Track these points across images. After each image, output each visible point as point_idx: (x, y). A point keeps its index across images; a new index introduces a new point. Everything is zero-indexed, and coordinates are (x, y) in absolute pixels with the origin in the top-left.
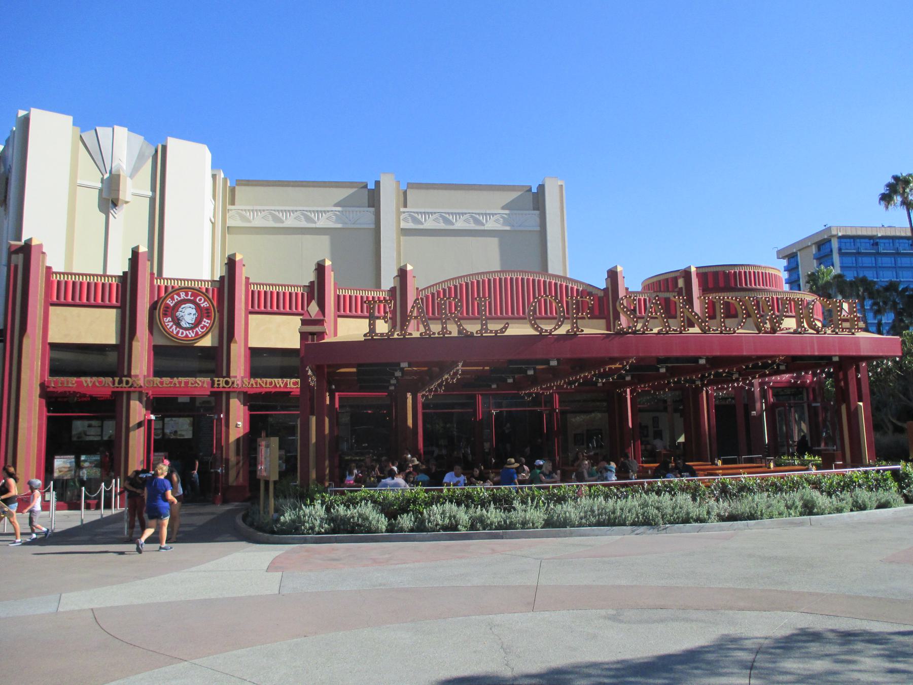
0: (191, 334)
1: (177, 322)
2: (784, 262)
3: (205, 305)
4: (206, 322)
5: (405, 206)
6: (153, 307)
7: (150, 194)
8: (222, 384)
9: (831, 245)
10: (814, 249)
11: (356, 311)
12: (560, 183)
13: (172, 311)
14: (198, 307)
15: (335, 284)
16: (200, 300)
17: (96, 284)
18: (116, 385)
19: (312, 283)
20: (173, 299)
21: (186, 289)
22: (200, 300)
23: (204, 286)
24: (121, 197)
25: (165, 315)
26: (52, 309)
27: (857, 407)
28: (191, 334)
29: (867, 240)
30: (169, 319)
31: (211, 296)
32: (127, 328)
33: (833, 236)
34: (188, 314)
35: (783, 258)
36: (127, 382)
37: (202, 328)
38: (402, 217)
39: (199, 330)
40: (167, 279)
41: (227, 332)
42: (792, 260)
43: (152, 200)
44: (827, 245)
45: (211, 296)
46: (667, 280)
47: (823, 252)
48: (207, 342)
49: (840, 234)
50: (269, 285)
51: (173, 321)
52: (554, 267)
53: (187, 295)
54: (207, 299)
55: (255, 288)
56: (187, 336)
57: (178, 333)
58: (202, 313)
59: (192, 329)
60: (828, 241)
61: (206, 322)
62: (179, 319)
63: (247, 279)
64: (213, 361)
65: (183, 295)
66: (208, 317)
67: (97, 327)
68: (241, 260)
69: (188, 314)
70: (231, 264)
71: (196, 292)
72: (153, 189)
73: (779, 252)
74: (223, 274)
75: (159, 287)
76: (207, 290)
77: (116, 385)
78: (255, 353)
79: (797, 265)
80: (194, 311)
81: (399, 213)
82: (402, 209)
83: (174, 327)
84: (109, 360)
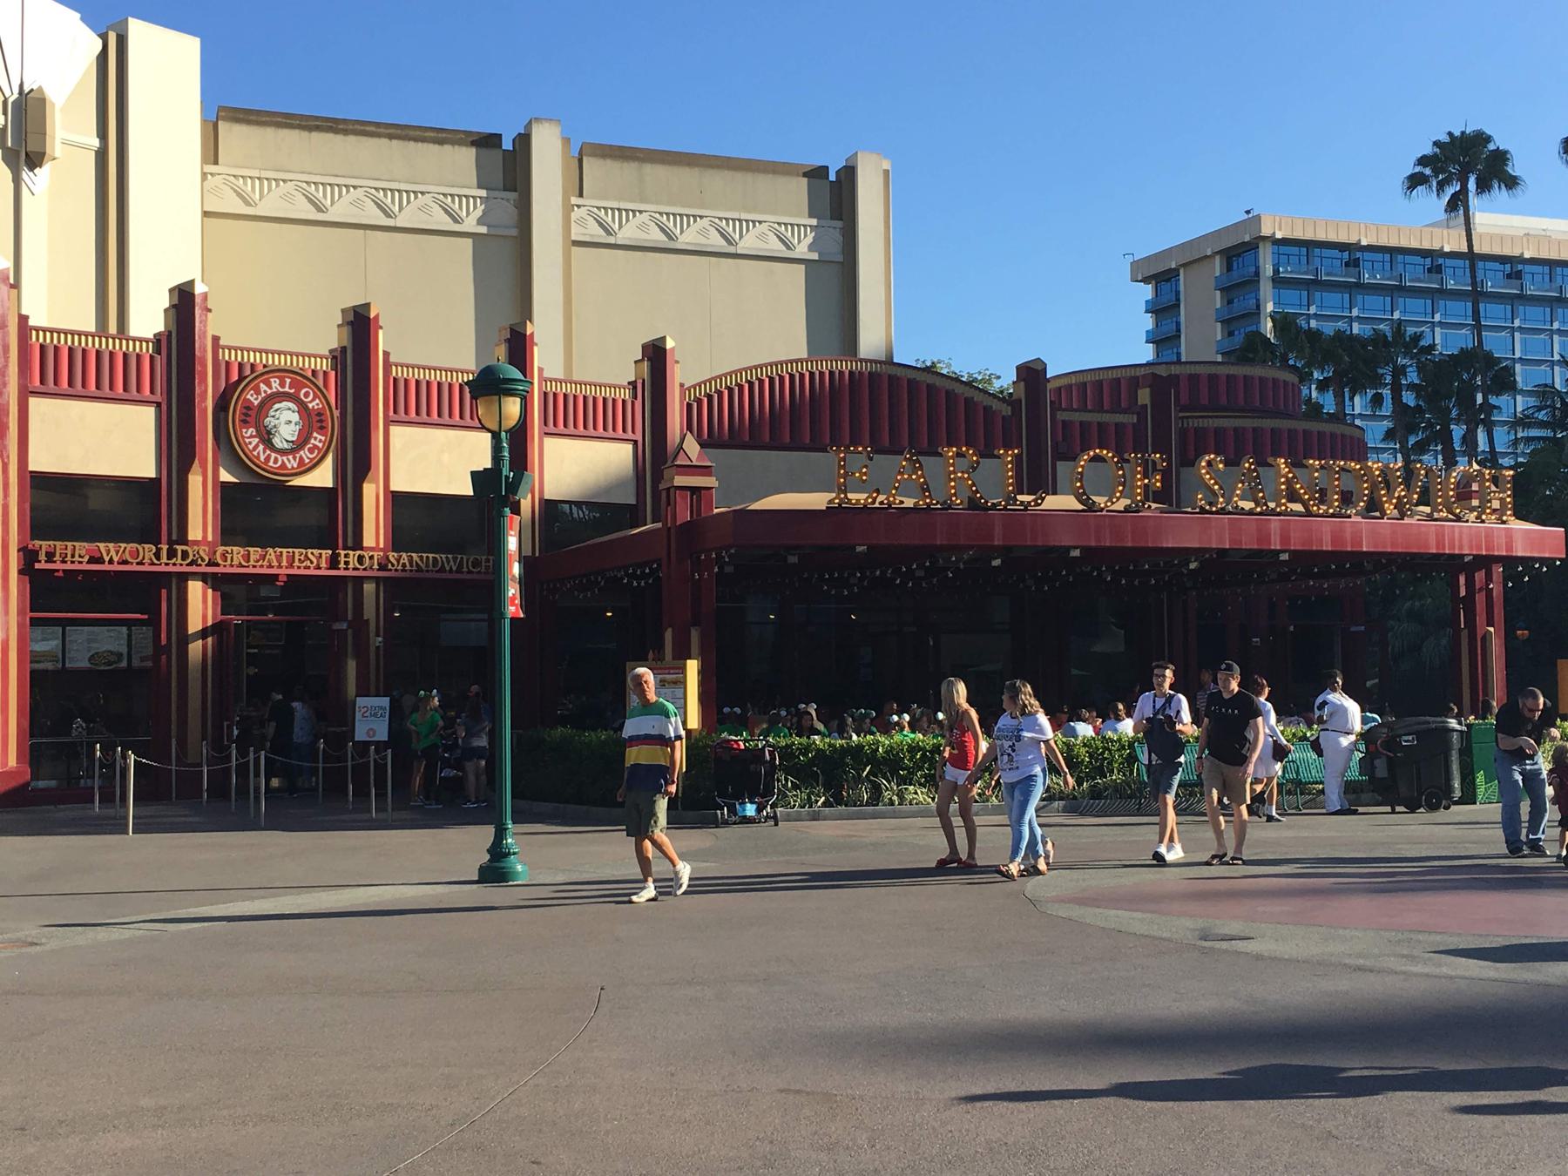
0: (291, 463)
1: (266, 437)
2: (1147, 291)
3: (315, 405)
4: (318, 439)
5: (581, 195)
6: (222, 405)
7: (96, 143)
8: (353, 562)
9: (1256, 259)
10: (1217, 266)
11: (406, 413)
12: (886, 165)
13: (256, 416)
14: (303, 408)
15: (1055, 445)
16: (307, 395)
17: (56, 348)
18: (164, 559)
19: (344, 349)
20: (258, 392)
21: (281, 372)
22: (307, 395)
23: (309, 364)
24: (48, 151)
25: (245, 422)
26: (33, 402)
27: (1486, 636)
28: (291, 463)
29: (1336, 253)
30: (252, 431)
31: (320, 383)
32: (177, 444)
33: (1264, 238)
34: (285, 422)
35: (1145, 280)
36: (185, 555)
37: (311, 451)
38: (574, 216)
39: (305, 454)
40: (134, 340)
41: (357, 458)
42: (1166, 287)
43: (101, 155)
44: (1249, 256)
45: (320, 383)
46: (1118, 380)
47: (1236, 276)
48: (322, 477)
49: (1279, 235)
50: (261, 352)
51: (259, 435)
52: (871, 340)
53: (282, 385)
54: (321, 393)
55: (233, 357)
56: (283, 466)
57: (268, 458)
58: (311, 421)
59: (293, 451)
60: (1252, 246)
61: (318, 439)
62: (269, 433)
64: (330, 518)
65: (275, 384)
66: (322, 429)
67: (109, 440)
69: (285, 422)
70: (360, 324)
71: (300, 378)
72: (102, 133)
73: (1135, 265)
74: (345, 343)
75: (228, 364)
76: (314, 372)
77: (164, 559)
78: (401, 503)
79: (1178, 300)
80: (295, 417)
81: (568, 208)
82: (574, 200)
83: (261, 447)
84: (143, 507)
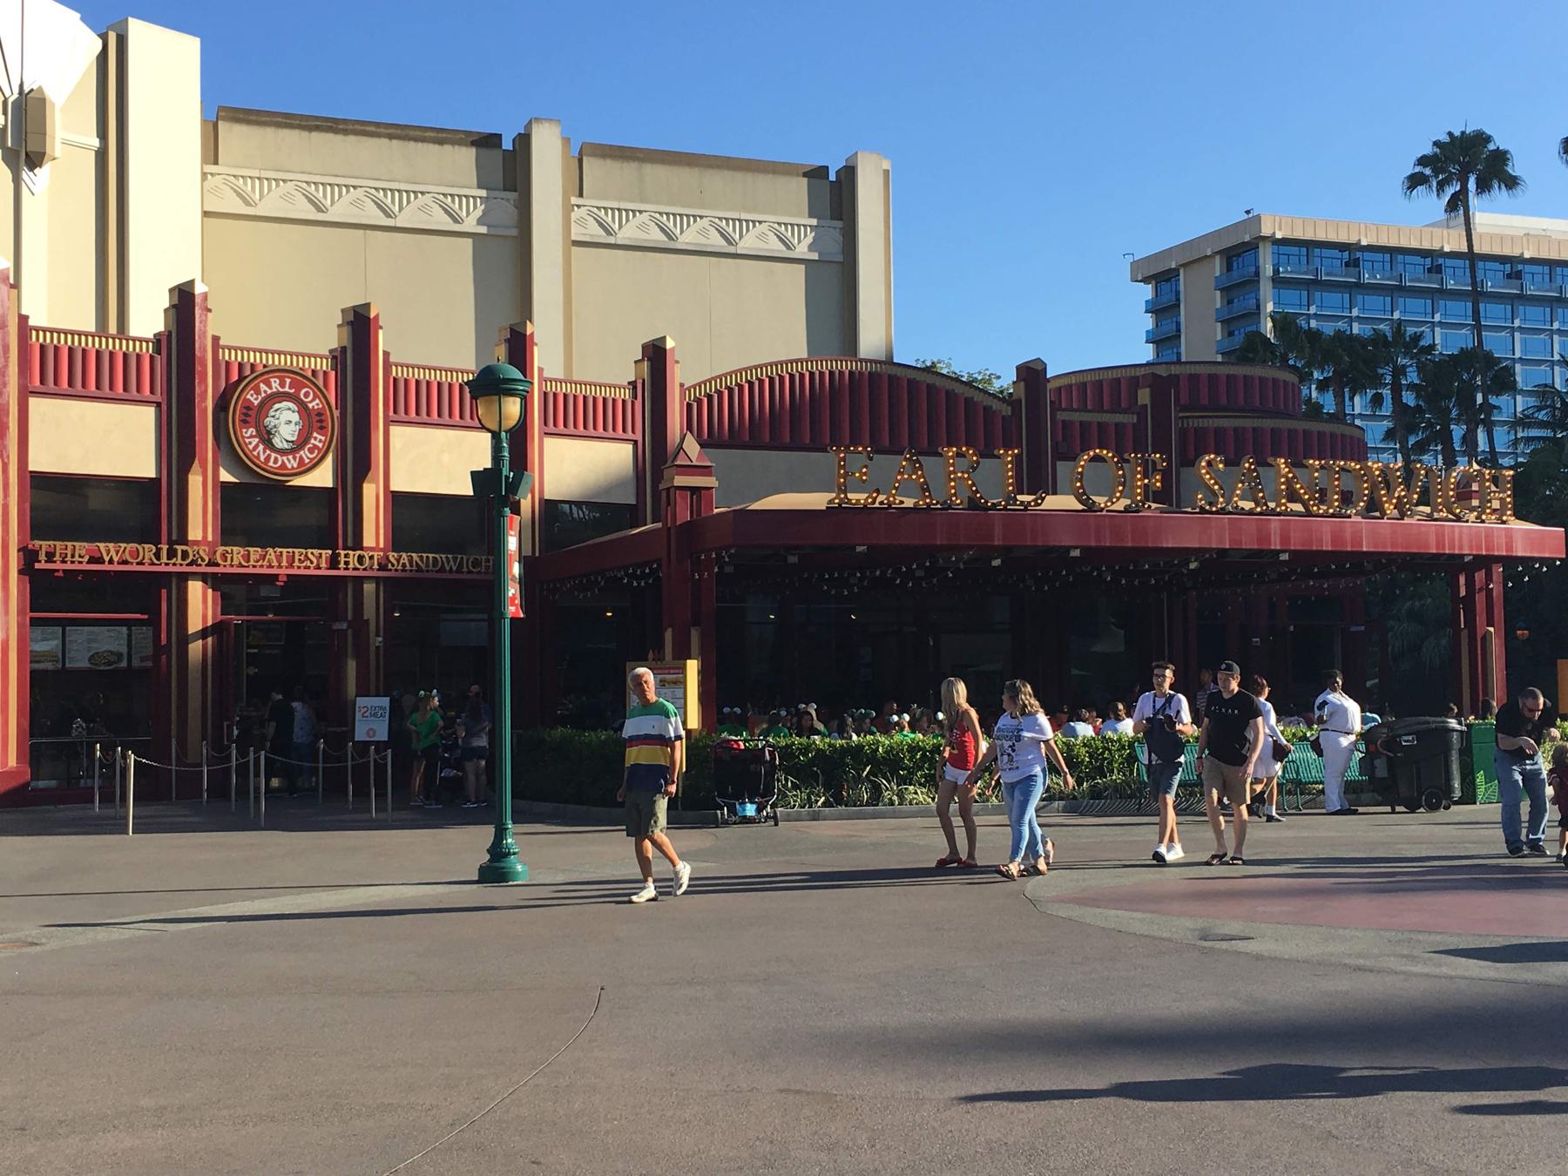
0: (291, 463)
1: (266, 437)
2: (1147, 291)
3: (315, 405)
4: (318, 439)
5: (581, 195)
6: (222, 405)
7: (96, 143)
8: (353, 562)
9: (1256, 259)
10: (1217, 266)
11: (406, 413)
12: (886, 165)
13: (256, 416)
14: (303, 408)
15: (1055, 445)
16: (307, 395)
17: (56, 348)
18: (164, 559)
19: (344, 349)
20: (258, 392)
21: (281, 372)
22: (307, 395)
23: (309, 364)
24: (48, 151)
25: (245, 422)
26: (33, 402)
27: (1486, 636)
28: (291, 463)
29: (1336, 253)
30: (252, 431)
31: (320, 383)
32: (177, 444)
33: (1264, 238)
34: (285, 422)
35: (1145, 280)
36: (185, 555)
37: (311, 451)
38: (574, 216)
39: (305, 454)
40: (134, 340)
41: (357, 458)
42: (1166, 287)
43: (101, 155)
44: (1249, 256)
45: (320, 383)
46: (1118, 380)
47: (1236, 276)
48: (322, 477)
49: (1279, 235)
50: (261, 352)
51: (259, 435)
52: (871, 340)
53: (282, 385)
54: (321, 393)
55: (233, 357)
56: (283, 466)
57: (268, 458)
58: (311, 421)
59: (293, 451)
60: (1252, 246)
61: (318, 439)
62: (269, 433)
63: (216, 339)
64: (330, 518)
65: (275, 384)
66: (322, 429)
67: (109, 440)
68: (205, 296)
69: (285, 422)
70: (360, 324)
71: (300, 378)
72: (102, 133)
73: (1135, 265)
74: (345, 343)
75: (228, 364)
76: (314, 372)
77: (164, 559)
78: (401, 503)
79: (1178, 300)
80: (295, 417)
81: (568, 208)
82: (574, 200)
83: (261, 447)
84: (143, 507)
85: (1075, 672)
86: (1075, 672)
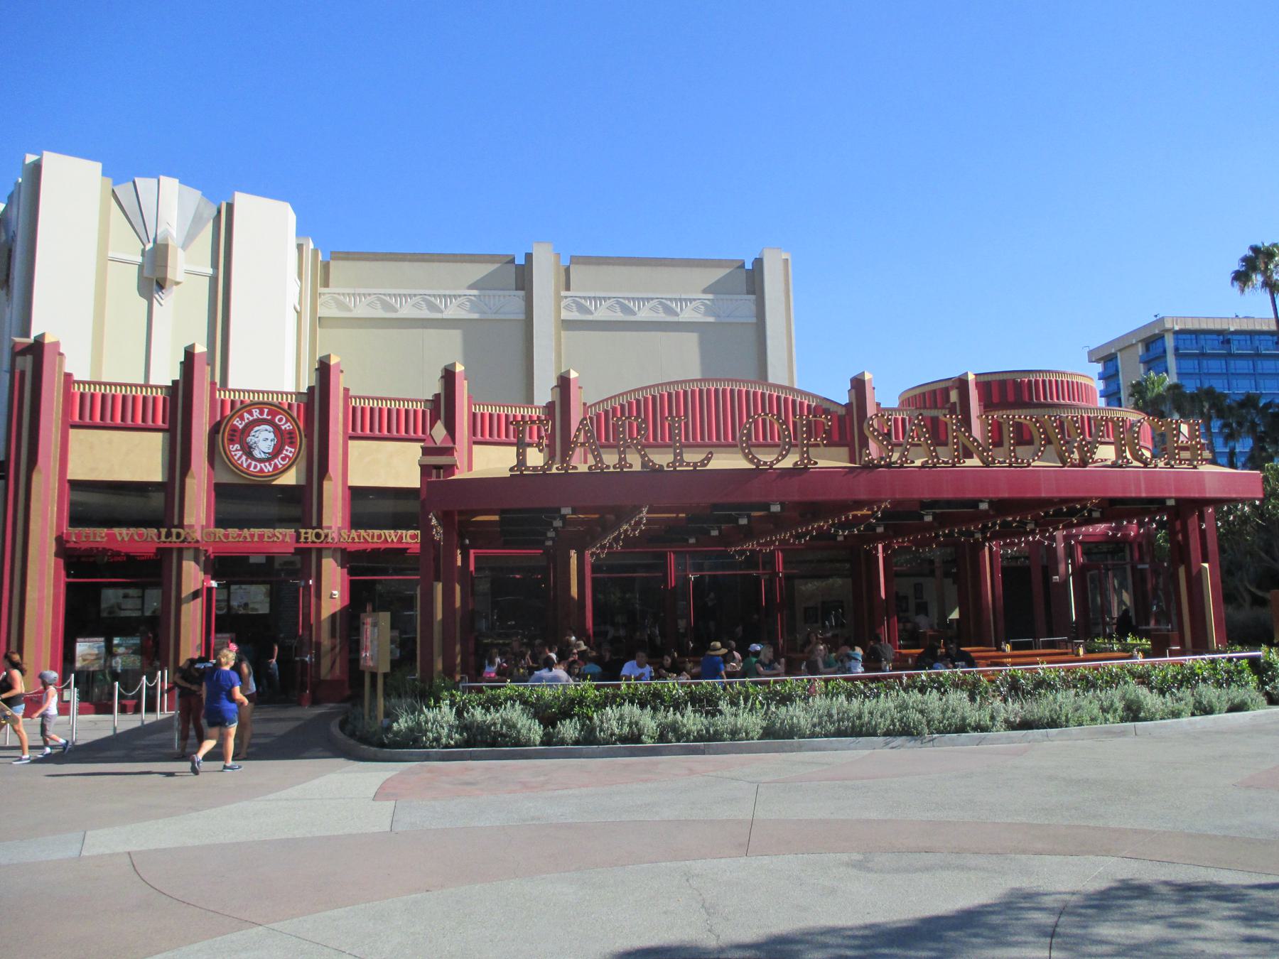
0: (268, 468)
1: (248, 451)
2: (1099, 367)
3: (287, 426)
4: (289, 451)
5: (568, 288)
6: (215, 430)
7: (210, 271)
8: (311, 537)
9: (1164, 343)
10: (1140, 349)
11: (499, 436)
12: (784, 256)
13: (240, 436)
14: (277, 430)
15: (470, 398)
16: (280, 420)
17: (134, 398)
18: (163, 539)
19: (437, 396)
20: (242, 418)
21: (260, 405)
22: (280, 420)
23: (285, 401)
24: (170, 276)
25: (232, 441)
26: (73, 433)
27: (1201, 570)
28: (268, 468)
29: (1215, 337)
30: (237, 446)
31: (295, 415)
32: (178, 459)
33: (1168, 330)
34: (263, 440)
35: (1097, 361)
36: (178, 535)
37: (283, 459)
38: (563, 304)
39: (279, 462)
40: (234, 391)
41: (318, 465)
42: (1110, 364)
43: (214, 280)
44: (1159, 343)
45: (295, 415)
46: (934, 391)
47: (1152, 353)
48: (290, 478)
49: (1177, 328)
50: (377, 399)
51: (242, 449)
52: (777, 374)
53: (262, 413)
54: (290, 418)
55: (358, 404)
56: (262, 470)
57: (249, 466)
58: (283, 439)
59: (269, 460)
60: (1160, 337)
61: (289, 451)
62: (250, 447)
64: (299, 505)
65: (256, 413)
66: (292, 444)
67: (136, 458)
69: (263, 440)
70: (324, 370)
71: (275, 409)
72: (215, 265)
73: (1091, 353)
74: (313, 384)
75: (223, 402)
76: (290, 405)
77: (163, 539)
78: (358, 494)
79: (1117, 371)
80: (272, 436)
81: (559, 299)
82: (563, 293)
83: (244, 458)
84: (152, 503)
85: (1147, 566)
86: (1147, 566)
